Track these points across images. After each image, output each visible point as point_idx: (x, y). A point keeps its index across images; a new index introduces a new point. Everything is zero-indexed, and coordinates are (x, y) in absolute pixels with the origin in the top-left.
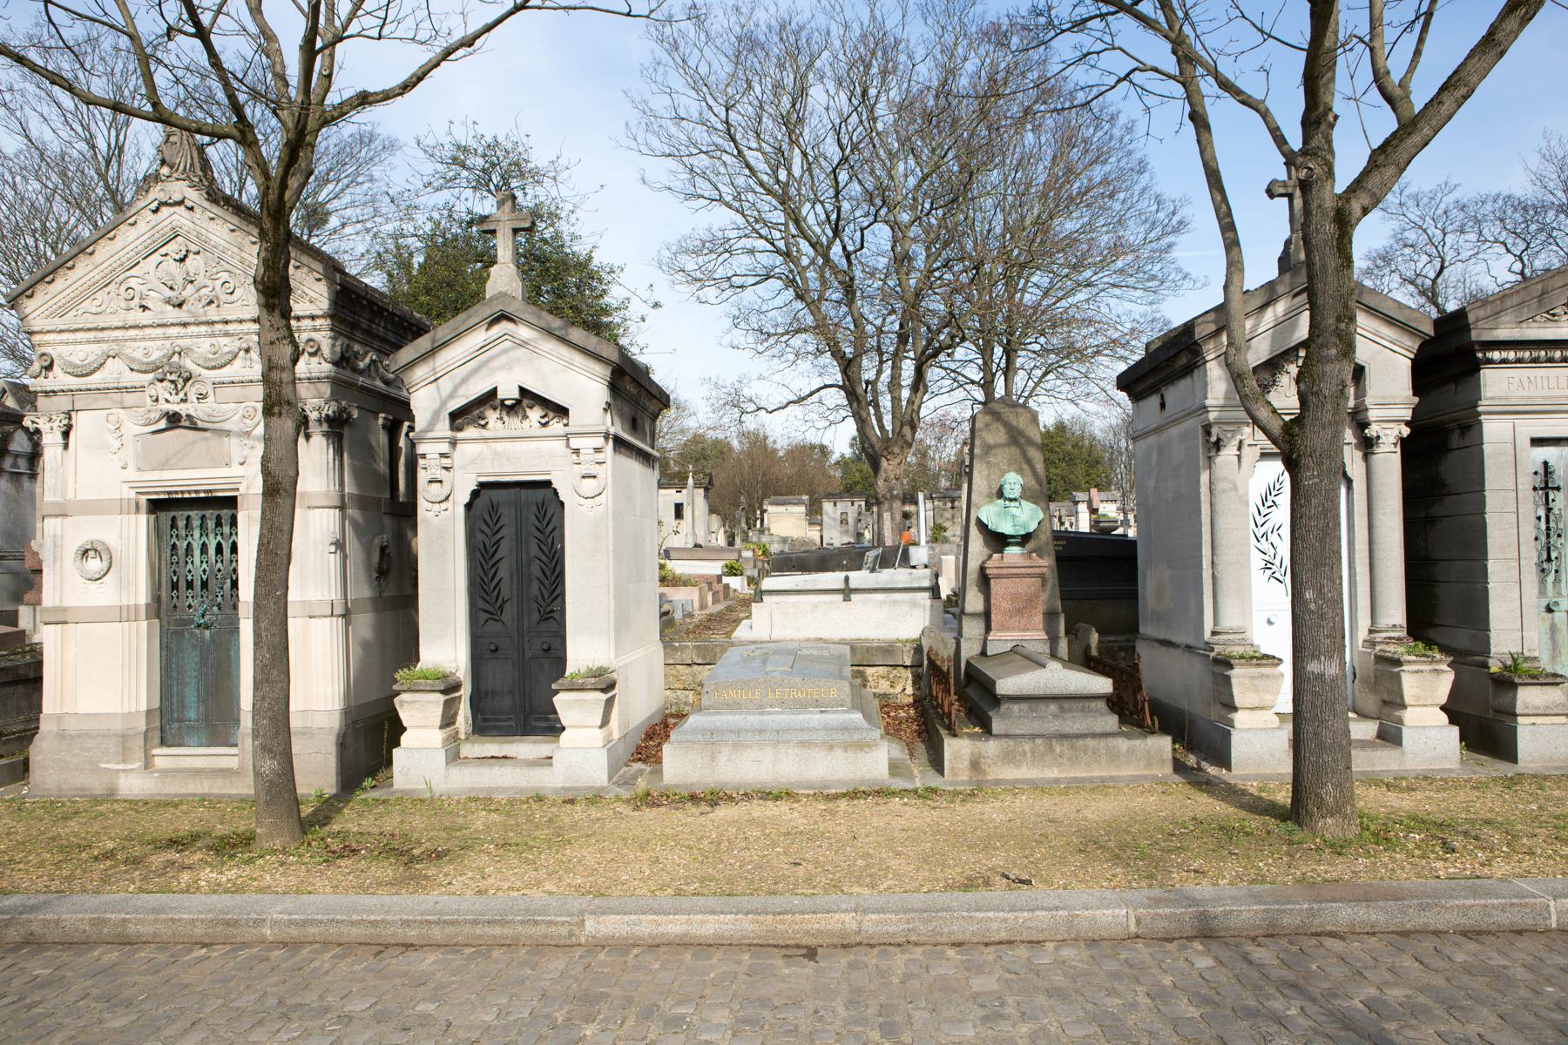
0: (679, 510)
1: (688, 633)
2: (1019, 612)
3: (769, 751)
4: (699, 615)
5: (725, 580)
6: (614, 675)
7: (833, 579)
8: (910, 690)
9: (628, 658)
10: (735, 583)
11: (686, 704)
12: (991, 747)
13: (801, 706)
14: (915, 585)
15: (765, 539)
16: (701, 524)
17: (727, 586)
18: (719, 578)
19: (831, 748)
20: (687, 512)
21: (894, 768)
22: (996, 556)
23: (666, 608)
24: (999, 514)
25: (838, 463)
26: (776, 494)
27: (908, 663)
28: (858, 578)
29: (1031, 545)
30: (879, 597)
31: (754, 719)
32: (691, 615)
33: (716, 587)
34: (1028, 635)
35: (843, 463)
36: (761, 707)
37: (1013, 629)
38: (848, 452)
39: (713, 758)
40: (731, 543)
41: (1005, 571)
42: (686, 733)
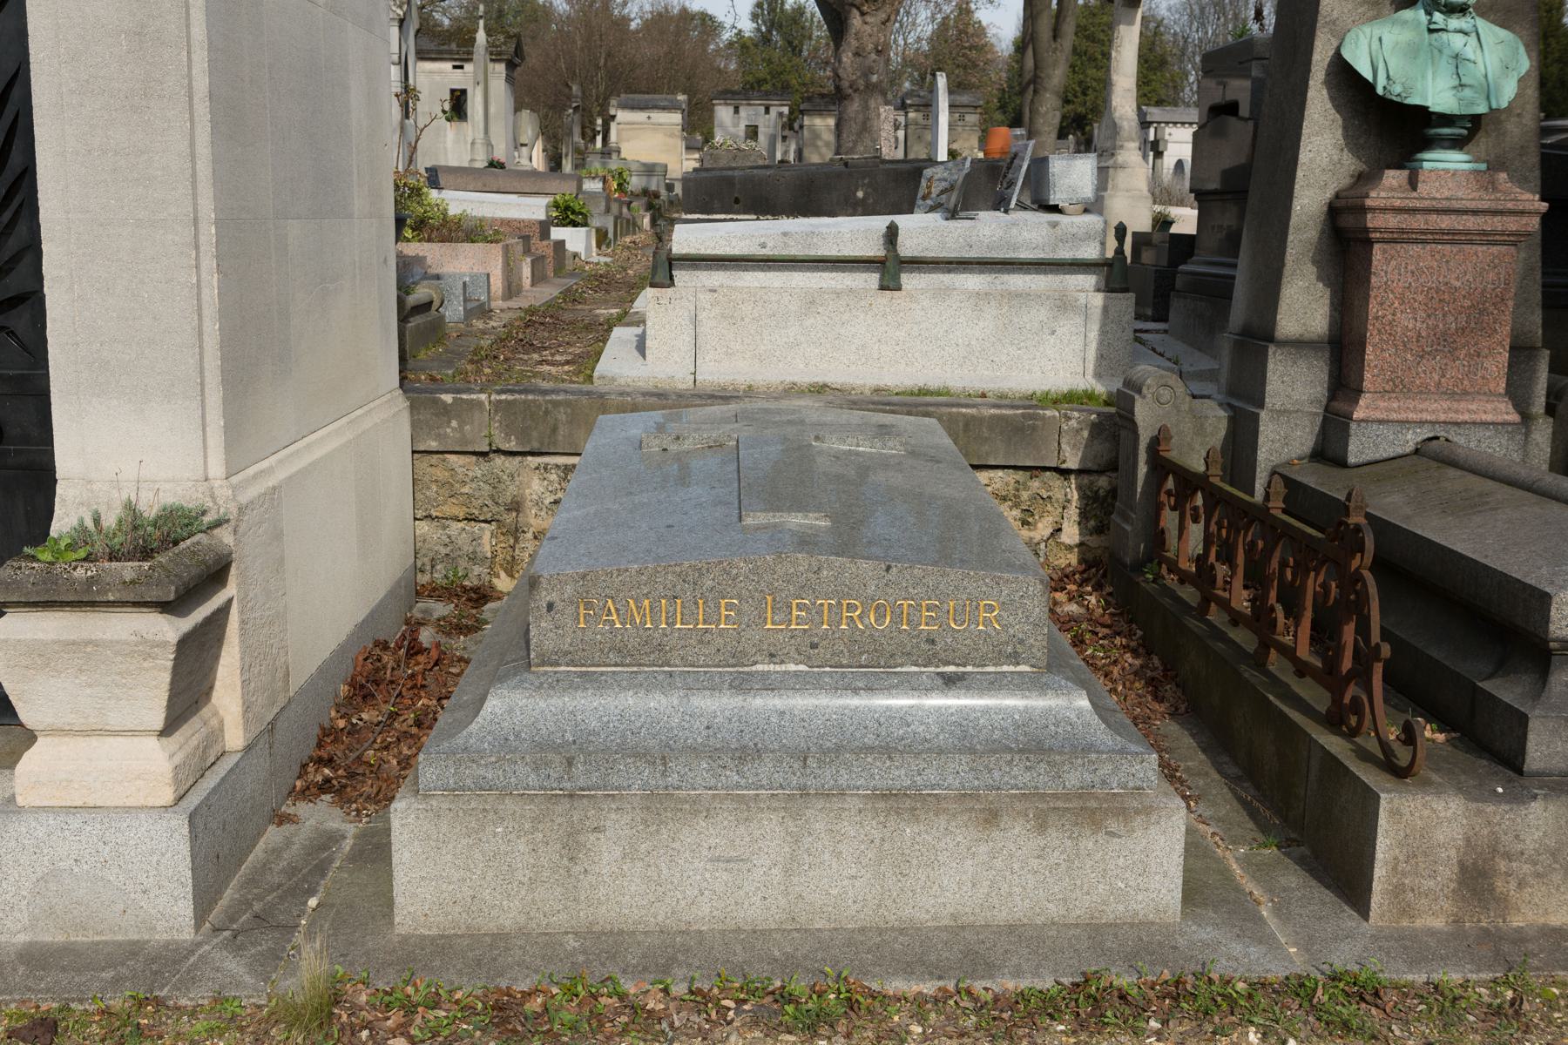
0: (458, 105)
1: (478, 358)
2: (1444, 343)
3: (770, 826)
4: (504, 311)
5: (557, 233)
6: (225, 536)
7: (855, 233)
8: (1071, 534)
9: (277, 468)
10: (576, 240)
11: (473, 558)
12: (1535, 822)
13: (874, 662)
14: (1065, 254)
15: (614, 164)
16: (496, 123)
17: (560, 245)
18: (544, 228)
19: (991, 817)
20: (475, 105)
21: (1202, 888)
22: (1394, 178)
23: (421, 293)
24: (1413, 51)
25: (731, 44)
26: (630, 90)
27: (1072, 463)
28: (921, 230)
29: (1483, 142)
30: (973, 282)
31: (717, 705)
32: (484, 311)
33: (540, 247)
34: (1471, 410)
35: (741, 46)
36: (739, 658)
37: (1423, 392)
38: (747, 26)
39: (572, 847)
40: (555, 162)
41: (1418, 222)
42: (472, 755)
